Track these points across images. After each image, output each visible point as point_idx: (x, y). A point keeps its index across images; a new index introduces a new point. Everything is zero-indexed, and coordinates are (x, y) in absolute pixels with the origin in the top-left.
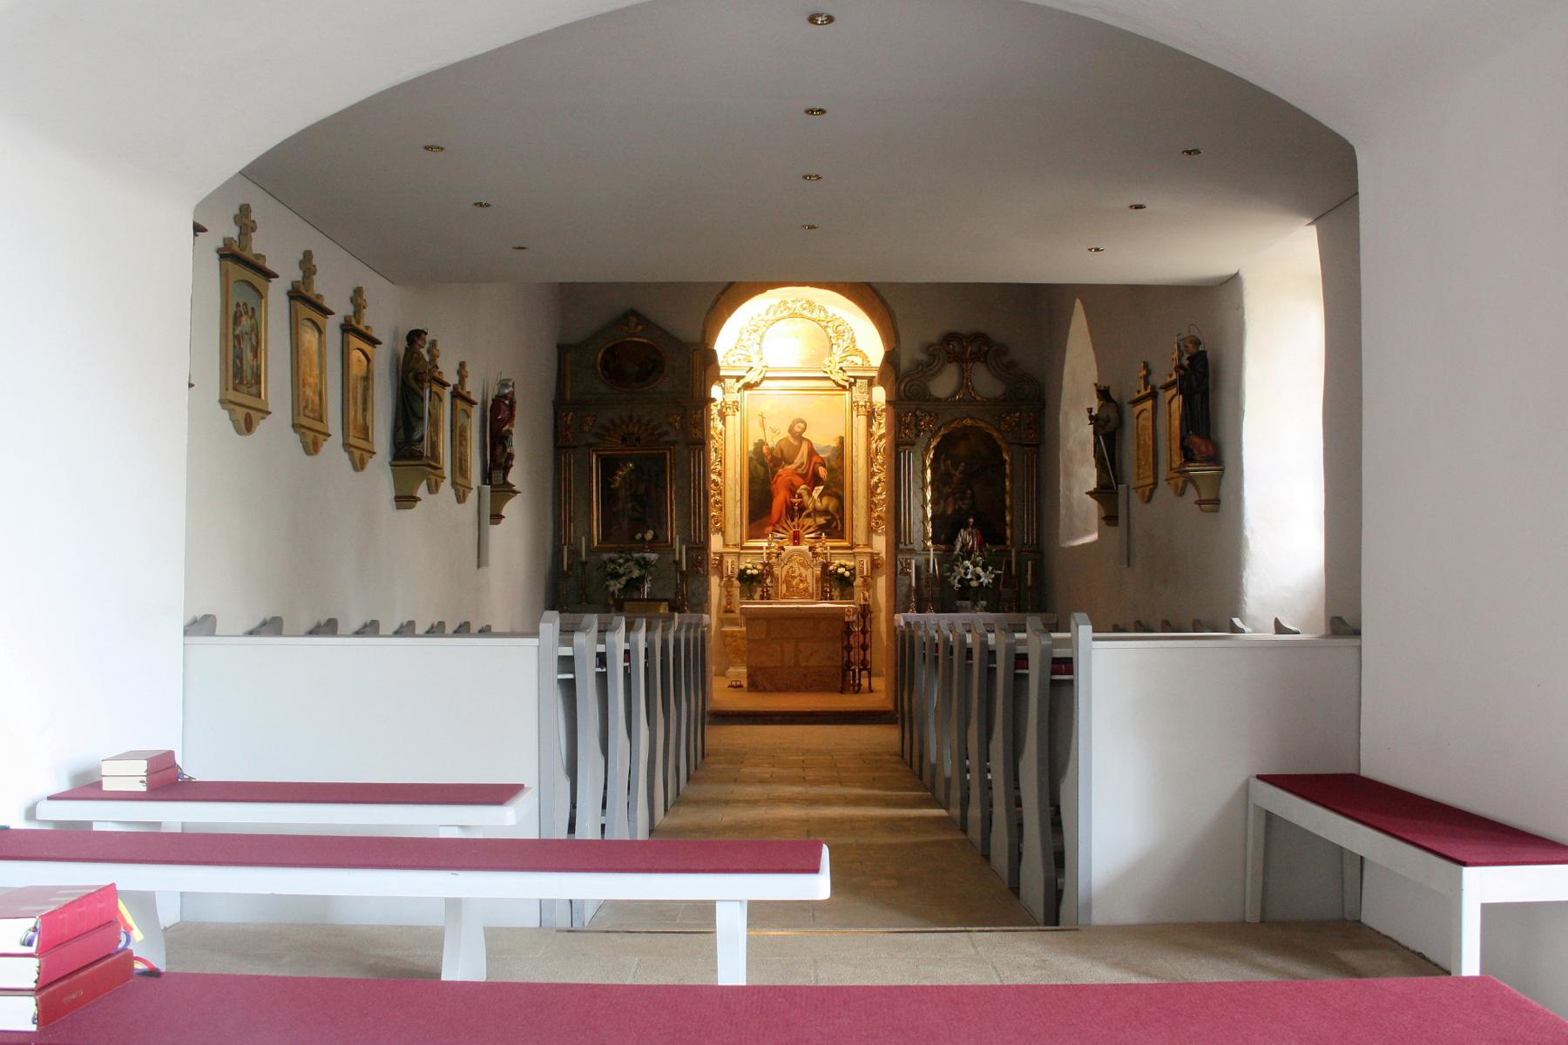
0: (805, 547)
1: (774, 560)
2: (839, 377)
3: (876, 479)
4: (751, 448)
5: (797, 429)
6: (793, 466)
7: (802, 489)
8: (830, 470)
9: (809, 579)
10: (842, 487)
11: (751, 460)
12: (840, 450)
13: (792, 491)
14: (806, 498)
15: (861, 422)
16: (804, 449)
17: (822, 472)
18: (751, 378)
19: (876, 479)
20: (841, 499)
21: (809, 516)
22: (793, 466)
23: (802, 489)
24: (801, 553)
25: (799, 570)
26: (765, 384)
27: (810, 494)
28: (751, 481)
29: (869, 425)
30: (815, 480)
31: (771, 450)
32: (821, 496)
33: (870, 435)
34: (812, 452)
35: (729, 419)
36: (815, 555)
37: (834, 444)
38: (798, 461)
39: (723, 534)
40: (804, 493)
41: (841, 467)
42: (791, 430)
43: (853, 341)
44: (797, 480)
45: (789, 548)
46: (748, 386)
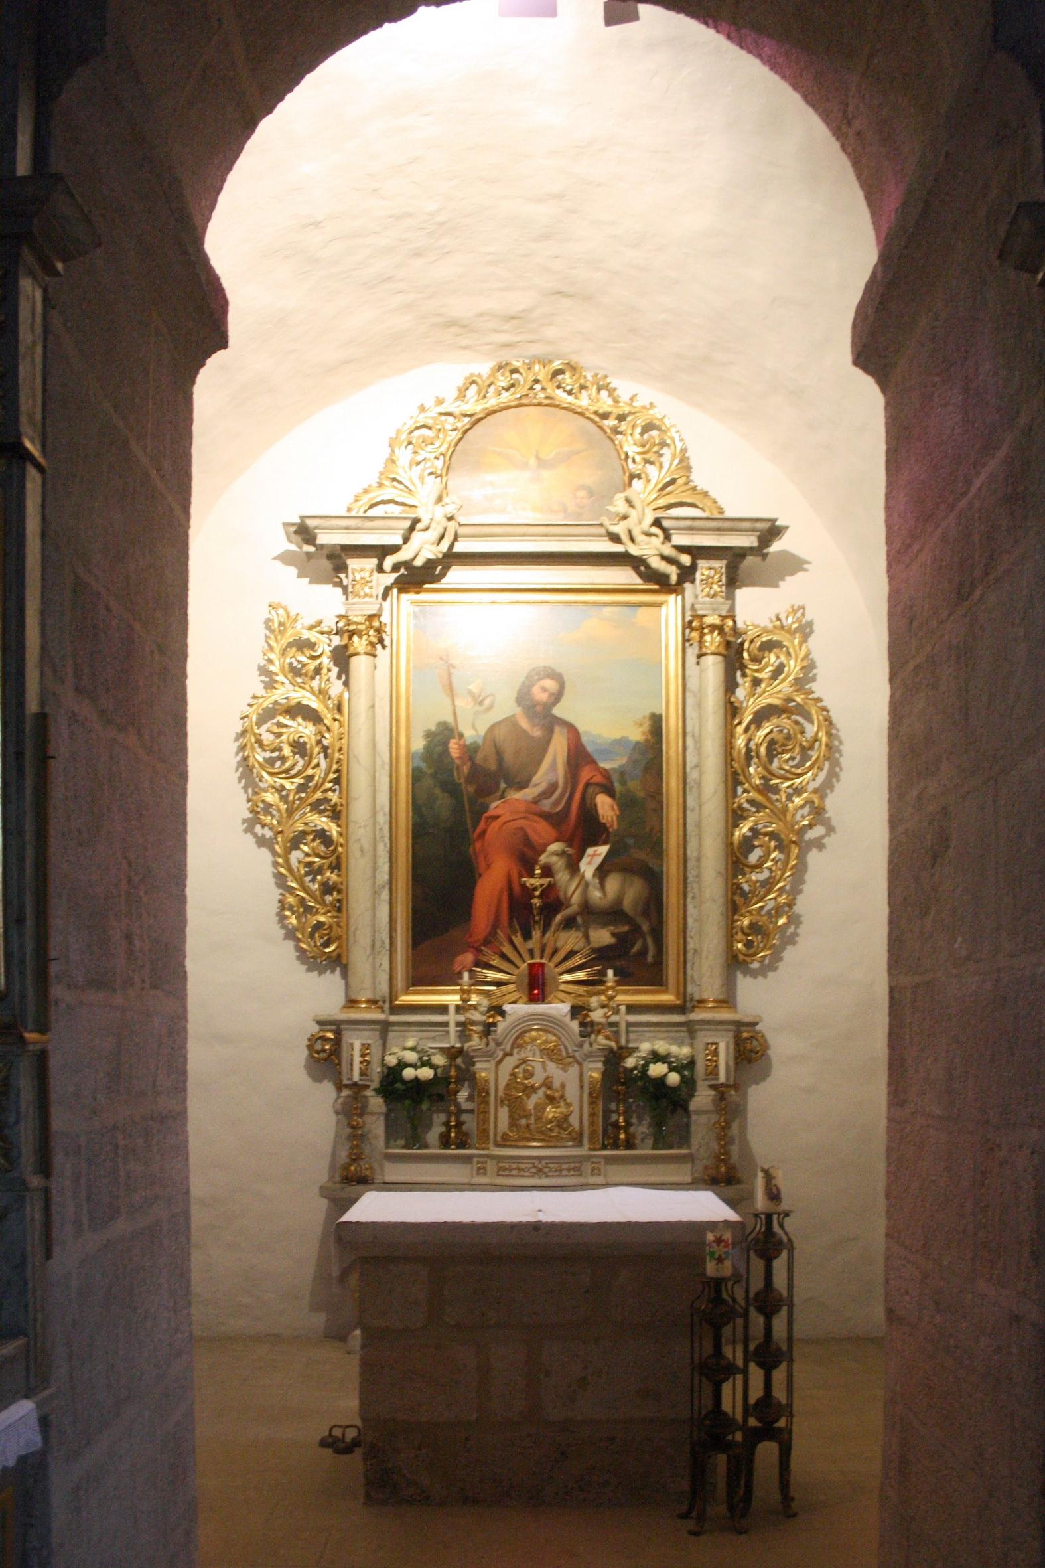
0: (559, 1008)
1: (476, 1042)
2: (650, 548)
3: (745, 829)
4: (419, 745)
5: (541, 696)
6: (529, 793)
7: (553, 852)
8: (627, 804)
9: (572, 1093)
10: (656, 846)
11: (417, 776)
12: (613, 935)
13: (526, 857)
14: (562, 876)
15: (713, 667)
16: (559, 747)
17: (605, 807)
18: (422, 548)
19: (745, 829)
20: (653, 880)
21: (569, 924)
22: (529, 793)
23: (553, 852)
24: (549, 1024)
25: (543, 1070)
26: (457, 575)
27: (573, 867)
28: (419, 832)
29: (730, 686)
30: (588, 830)
31: (470, 752)
32: (602, 871)
33: (732, 710)
34: (579, 756)
35: (359, 665)
36: (588, 1028)
37: (637, 735)
38: (541, 778)
39: (345, 975)
40: (558, 863)
41: (656, 794)
42: (524, 698)
43: (685, 465)
44: (540, 830)
45: (518, 1009)
46: (416, 578)
